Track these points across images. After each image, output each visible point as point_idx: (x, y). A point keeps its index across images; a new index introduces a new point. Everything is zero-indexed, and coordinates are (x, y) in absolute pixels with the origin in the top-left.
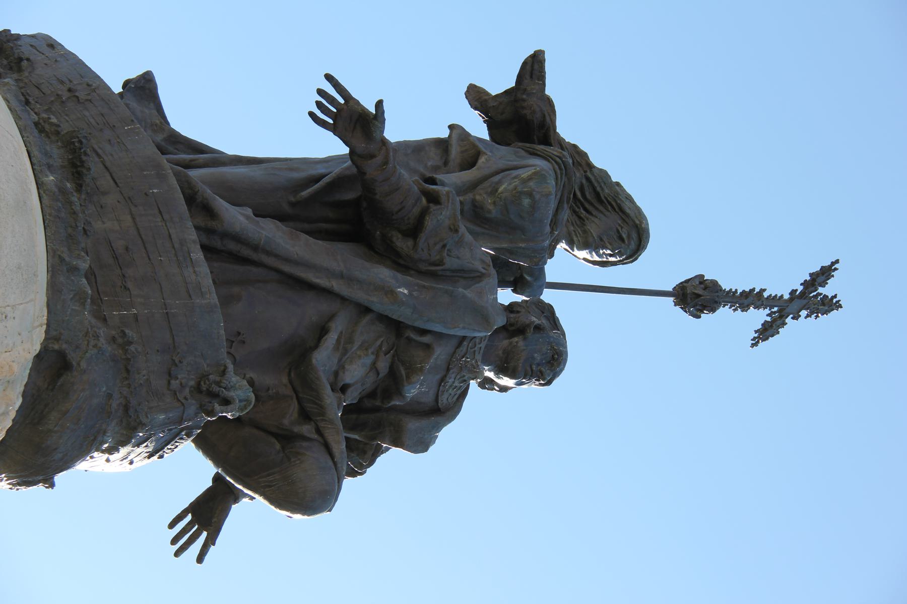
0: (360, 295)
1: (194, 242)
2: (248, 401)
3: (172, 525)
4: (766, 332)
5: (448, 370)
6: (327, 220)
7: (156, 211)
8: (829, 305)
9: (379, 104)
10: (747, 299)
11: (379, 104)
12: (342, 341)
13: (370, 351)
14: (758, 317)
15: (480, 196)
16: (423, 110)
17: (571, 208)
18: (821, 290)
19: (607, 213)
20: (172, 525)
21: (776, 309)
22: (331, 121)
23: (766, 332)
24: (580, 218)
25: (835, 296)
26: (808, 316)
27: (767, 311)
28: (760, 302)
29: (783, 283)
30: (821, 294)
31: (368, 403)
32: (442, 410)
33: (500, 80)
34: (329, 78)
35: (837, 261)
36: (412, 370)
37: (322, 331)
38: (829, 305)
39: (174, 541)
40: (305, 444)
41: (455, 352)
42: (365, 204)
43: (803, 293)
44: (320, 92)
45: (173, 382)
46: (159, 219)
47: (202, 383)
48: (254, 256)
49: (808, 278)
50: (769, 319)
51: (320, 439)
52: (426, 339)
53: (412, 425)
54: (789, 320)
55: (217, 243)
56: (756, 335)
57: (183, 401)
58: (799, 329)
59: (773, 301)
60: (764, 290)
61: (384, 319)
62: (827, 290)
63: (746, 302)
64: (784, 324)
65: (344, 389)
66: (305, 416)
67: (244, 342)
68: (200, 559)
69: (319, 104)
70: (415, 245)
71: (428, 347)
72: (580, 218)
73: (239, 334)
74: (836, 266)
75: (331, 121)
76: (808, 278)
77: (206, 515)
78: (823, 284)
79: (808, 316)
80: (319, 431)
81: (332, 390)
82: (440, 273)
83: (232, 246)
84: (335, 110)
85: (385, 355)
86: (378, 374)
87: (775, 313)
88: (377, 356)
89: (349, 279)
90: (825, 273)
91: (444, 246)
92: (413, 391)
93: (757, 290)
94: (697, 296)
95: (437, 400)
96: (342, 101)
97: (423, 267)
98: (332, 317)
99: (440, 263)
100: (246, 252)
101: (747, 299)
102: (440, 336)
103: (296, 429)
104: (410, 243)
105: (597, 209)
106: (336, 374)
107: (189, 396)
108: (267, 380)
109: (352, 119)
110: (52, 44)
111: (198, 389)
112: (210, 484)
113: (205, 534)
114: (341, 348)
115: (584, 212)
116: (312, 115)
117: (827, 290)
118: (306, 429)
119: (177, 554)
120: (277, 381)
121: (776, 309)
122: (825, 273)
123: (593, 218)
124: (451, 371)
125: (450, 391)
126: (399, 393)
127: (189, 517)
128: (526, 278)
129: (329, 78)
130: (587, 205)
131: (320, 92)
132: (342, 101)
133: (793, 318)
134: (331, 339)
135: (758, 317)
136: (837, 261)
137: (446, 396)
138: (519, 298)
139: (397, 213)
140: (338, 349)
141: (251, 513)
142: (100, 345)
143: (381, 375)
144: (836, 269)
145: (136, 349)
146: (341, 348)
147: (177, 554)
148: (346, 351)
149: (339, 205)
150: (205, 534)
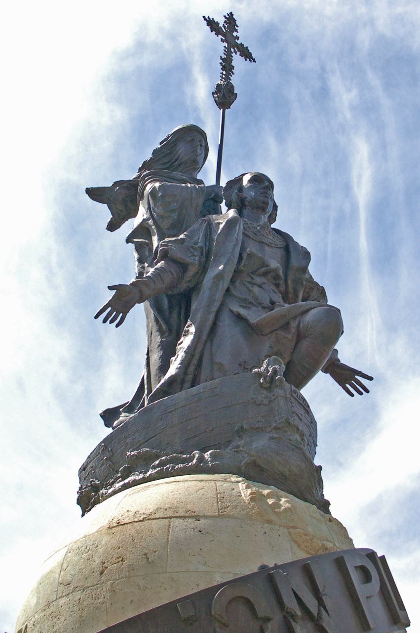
0: (219, 296)
1: (186, 392)
2: (275, 360)
3: (352, 395)
4: (247, 54)
5: (263, 242)
6: (179, 314)
7: (170, 415)
8: (230, 20)
9: (110, 288)
10: (227, 66)
11: (110, 288)
12: (245, 305)
13: (251, 288)
14: (237, 60)
15: (165, 225)
16: (118, 259)
17: (174, 170)
18: (221, 25)
19: (177, 149)
20: (352, 395)
21: (232, 50)
22: (121, 314)
23: (247, 54)
24: (180, 165)
25: (225, 16)
26: (225, 47)
27: (234, 55)
28: (228, 59)
29: (219, 46)
30: (224, 25)
31: (282, 288)
32: (286, 242)
33: (104, 213)
34: (96, 317)
35: (204, 17)
36: (264, 264)
37: (239, 317)
38: (230, 20)
39: (361, 393)
40: (301, 325)
41: (253, 239)
42: (170, 292)
43: (224, 35)
44: (105, 321)
45: (264, 402)
46: (174, 413)
47: (265, 386)
48: (197, 357)
49: (214, 32)
50: (238, 53)
51: (299, 317)
52: (245, 256)
53: (295, 262)
54: (239, 42)
55: (190, 377)
56: (248, 59)
57: (275, 396)
58: (243, 35)
59: (228, 53)
60: (221, 57)
61: (232, 281)
62: (221, 21)
63: (228, 67)
64: (242, 45)
65: (273, 303)
66: (286, 326)
67: (245, 361)
68: (371, 379)
69: (111, 322)
70: (192, 264)
71: (250, 256)
72: (180, 165)
73: (240, 364)
74: (207, 17)
75: (121, 314)
76: (214, 32)
77: (348, 378)
78: (218, 24)
79: (237, 31)
80: (295, 318)
81: (273, 310)
82: (207, 248)
83: (192, 369)
84: (115, 313)
85: (253, 279)
86: (264, 283)
87: (235, 50)
88: (255, 284)
89: (211, 300)
90: (211, 23)
91: (192, 247)
92: (275, 264)
93: (221, 61)
94: (224, 96)
95: (281, 248)
96: (110, 309)
97: (203, 259)
98: (231, 311)
99: (201, 248)
100: (195, 361)
101: (227, 66)
102: (243, 249)
103: (293, 331)
104: (190, 267)
105: (174, 155)
106: (264, 308)
107: (273, 394)
108: (266, 349)
109: (120, 304)
110: (83, 469)
111: (269, 389)
112: (328, 375)
113: (356, 377)
114: (248, 306)
115: (176, 163)
116: (117, 326)
117: (221, 21)
118: (294, 325)
119: (367, 391)
120: (266, 345)
121: (232, 50)
122: (211, 23)
123: (180, 158)
124: (263, 240)
125: (275, 240)
126: (275, 270)
127: (348, 386)
128: (211, 199)
129: (96, 317)
130: (172, 162)
131: (105, 321)
132: (110, 309)
133: (238, 40)
134: (243, 312)
135: (237, 60)
136: (204, 17)
137: (278, 243)
138: (224, 201)
139: (172, 274)
140: (249, 307)
141: (347, 351)
142: (242, 445)
143: (265, 281)
144: (209, 17)
145: (245, 424)
146: (248, 306)
147: (367, 391)
148: (250, 303)
149: (171, 307)
150: (356, 377)
